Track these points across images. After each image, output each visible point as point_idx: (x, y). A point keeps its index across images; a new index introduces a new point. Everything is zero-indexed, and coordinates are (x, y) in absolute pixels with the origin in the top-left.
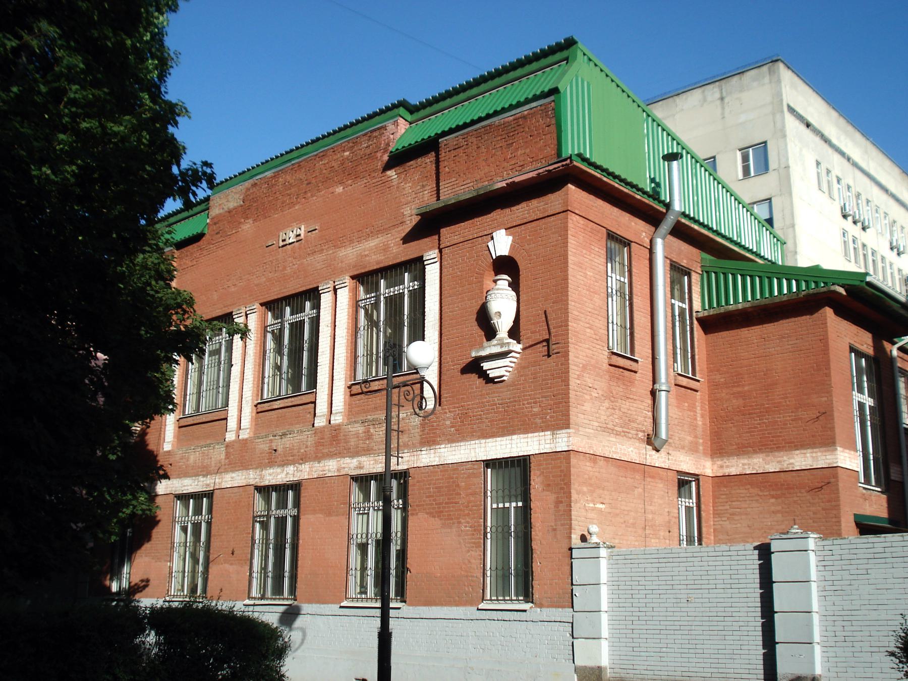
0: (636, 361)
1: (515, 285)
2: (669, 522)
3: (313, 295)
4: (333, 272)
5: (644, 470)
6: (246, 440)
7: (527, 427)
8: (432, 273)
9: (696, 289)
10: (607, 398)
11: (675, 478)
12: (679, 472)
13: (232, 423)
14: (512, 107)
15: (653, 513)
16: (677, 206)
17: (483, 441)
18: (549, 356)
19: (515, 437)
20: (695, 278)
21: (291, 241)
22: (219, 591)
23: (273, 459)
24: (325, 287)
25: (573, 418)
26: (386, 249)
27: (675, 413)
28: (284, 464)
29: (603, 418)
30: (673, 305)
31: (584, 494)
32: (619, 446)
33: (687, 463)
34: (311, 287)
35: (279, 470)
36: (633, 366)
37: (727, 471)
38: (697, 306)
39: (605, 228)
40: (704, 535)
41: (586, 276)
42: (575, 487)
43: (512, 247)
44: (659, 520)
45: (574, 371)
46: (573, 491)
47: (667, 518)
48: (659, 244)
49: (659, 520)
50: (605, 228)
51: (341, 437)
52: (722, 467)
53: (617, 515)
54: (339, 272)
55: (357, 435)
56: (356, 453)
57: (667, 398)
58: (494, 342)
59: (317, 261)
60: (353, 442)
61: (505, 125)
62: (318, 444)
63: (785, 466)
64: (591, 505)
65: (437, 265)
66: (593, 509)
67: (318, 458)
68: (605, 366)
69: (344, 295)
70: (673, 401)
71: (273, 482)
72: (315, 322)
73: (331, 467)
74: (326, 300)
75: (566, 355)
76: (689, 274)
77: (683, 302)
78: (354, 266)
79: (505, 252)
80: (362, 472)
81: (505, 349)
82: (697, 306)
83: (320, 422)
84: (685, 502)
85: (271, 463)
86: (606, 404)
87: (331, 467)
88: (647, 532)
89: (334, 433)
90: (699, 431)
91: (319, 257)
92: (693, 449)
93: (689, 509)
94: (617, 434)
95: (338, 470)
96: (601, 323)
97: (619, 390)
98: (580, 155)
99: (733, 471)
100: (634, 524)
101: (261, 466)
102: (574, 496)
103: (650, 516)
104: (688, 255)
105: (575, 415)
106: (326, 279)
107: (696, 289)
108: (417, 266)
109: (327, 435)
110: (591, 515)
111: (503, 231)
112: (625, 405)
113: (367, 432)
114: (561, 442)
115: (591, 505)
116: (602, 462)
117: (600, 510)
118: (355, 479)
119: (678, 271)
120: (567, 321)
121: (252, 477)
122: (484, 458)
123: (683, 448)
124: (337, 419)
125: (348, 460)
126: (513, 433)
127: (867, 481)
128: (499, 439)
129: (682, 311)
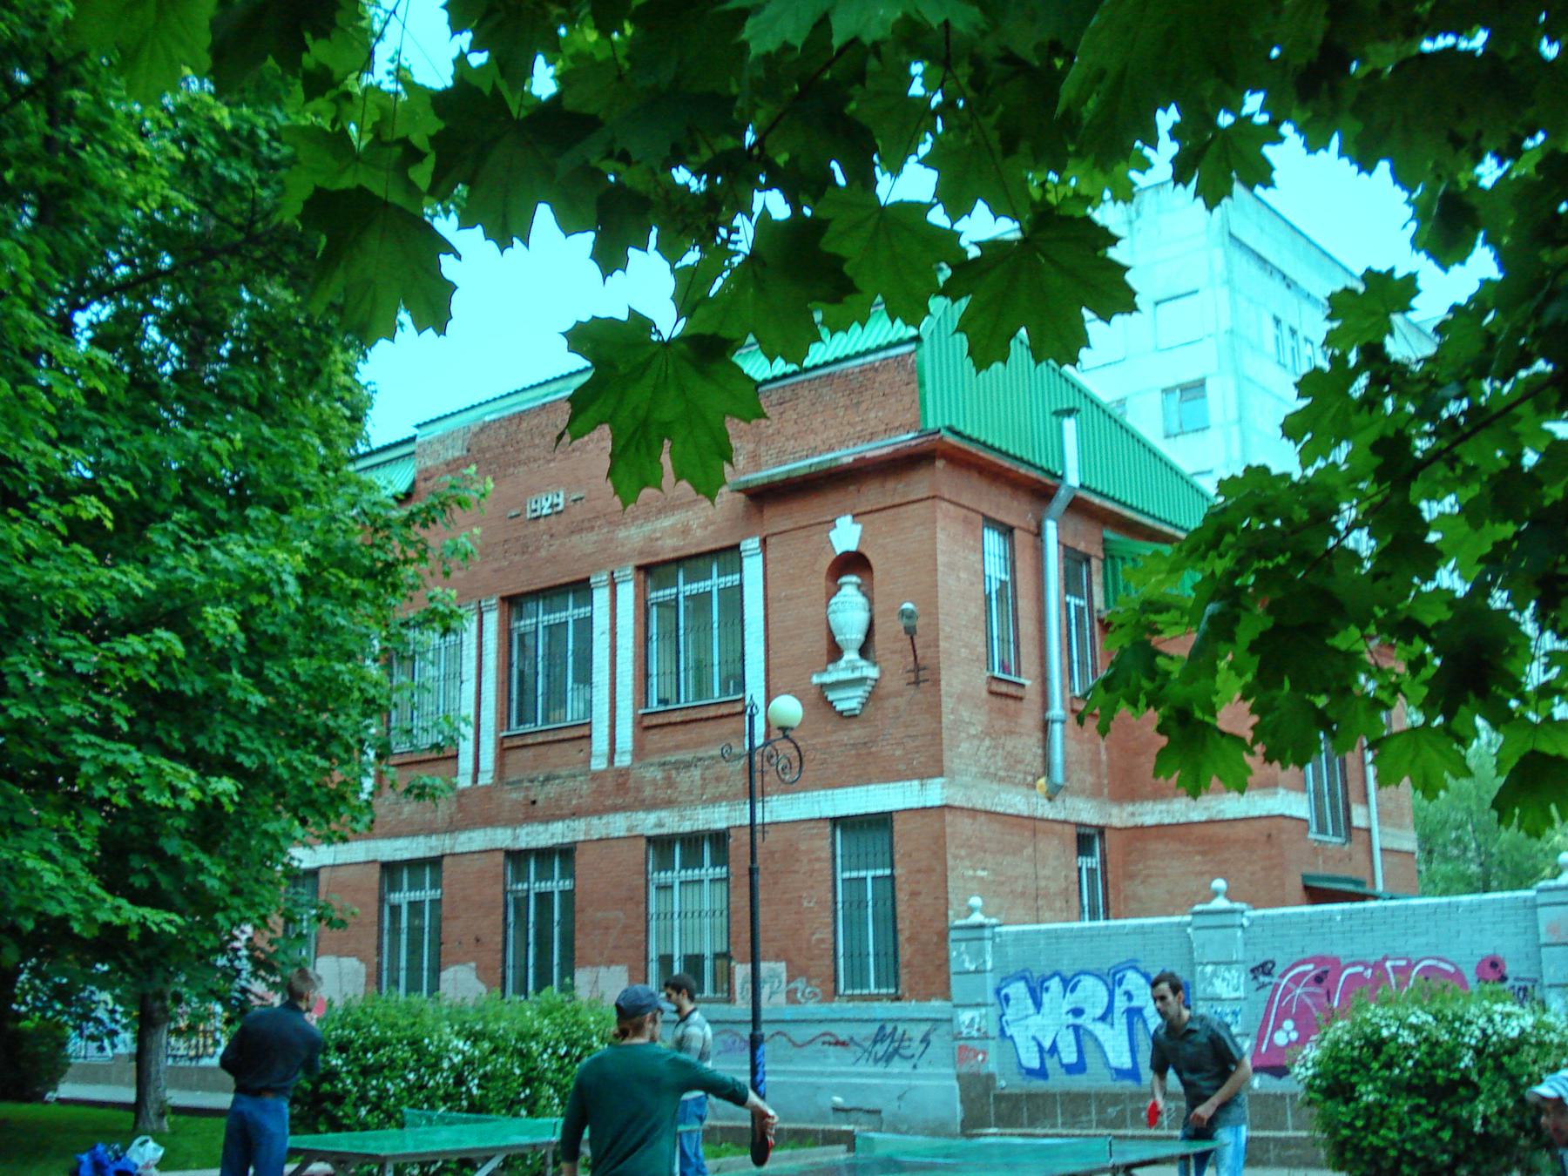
0: (1022, 685)
1: (867, 591)
2: (1067, 889)
3: (581, 589)
4: (610, 559)
5: (1031, 824)
6: (487, 787)
7: (890, 775)
8: (753, 567)
9: (1097, 580)
10: (988, 734)
11: (1071, 832)
12: (1079, 825)
13: (466, 763)
14: (858, 355)
15: (1048, 878)
16: (1073, 479)
17: (830, 792)
18: (917, 683)
19: (872, 787)
20: (1095, 563)
21: (545, 511)
22: (932, 1038)
23: (532, 812)
24: (599, 579)
25: (946, 763)
26: (686, 531)
27: (1074, 747)
28: (548, 819)
29: (984, 761)
30: (1068, 605)
31: (962, 858)
32: (1003, 796)
33: (1087, 812)
34: (578, 577)
35: (541, 828)
36: (1019, 692)
37: (1139, 821)
38: (1098, 601)
39: (977, 512)
40: (1111, 904)
41: (959, 579)
42: (951, 850)
43: (862, 540)
44: (1053, 887)
45: (947, 704)
46: (949, 857)
47: (1064, 885)
48: (1051, 529)
49: (1053, 887)
50: (977, 512)
51: (631, 783)
52: (1133, 814)
53: (1002, 883)
54: (621, 560)
55: (654, 782)
56: (651, 806)
57: (1063, 730)
58: (842, 663)
59: (585, 542)
60: (648, 791)
61: (845, 376)
62: (599, 792)
63: (1214, 814)
64: (971, 873)
65: (760, 558)
66: (974, 877)
67: (599, 812)
68: (984, 694)
69: (627, 593)
70: (1070, 733)
71: (533, 845)
72: (585, 625)
73: (617, 825)
74: (601, 597)
75: (937, 682)
76: (1087, 559)
77: (1081, 597)
78: (641, 553)
79: (853, 547)
80: (664, 831)
81: (857, 674)
82: (1098, 601)
83: (599, 764)
84: (1086, 862)
85: (529, 819)
86: (987, 742)
87: (617, 825)
88: (1040, 903)
89: (620, 780)
90: (1104, 769)
91: (591, 537)
92: (1095, 793)
93: (1091, 871)
94: (1001, 780)
95: (629, 829)
96: (979, 639)
97: (1001, 723)
98: (951, 429)
99: (1149, 820)
100: (1023, 894)
101: (513, 822)
102: (950, 862)
103: (1043, 883)
104: (1088, 540)
105: (951, 760)
106: (598, 567)
107: (1097, 580)
108: (729, 555)
109: (609, 784)
110: (973, 885)
111: (849, 518)
112: (1009, 745)
113: (668, 778)
114: (934, 793)
115: (971, 873)
116: (982, 818)
117: (982, 878)
118: (651, 840)
119: (1074, 560)
120: (937, 639)
121: (503, 838)
122: (831, 814)
123: (1083, 792)
124: (623, 760)
125: (641, 815)
126: (869, 782)
127: (1322, 829)
128: (850, 790)
129: (1079, 610)
